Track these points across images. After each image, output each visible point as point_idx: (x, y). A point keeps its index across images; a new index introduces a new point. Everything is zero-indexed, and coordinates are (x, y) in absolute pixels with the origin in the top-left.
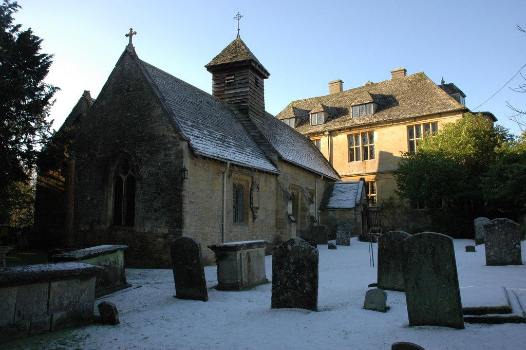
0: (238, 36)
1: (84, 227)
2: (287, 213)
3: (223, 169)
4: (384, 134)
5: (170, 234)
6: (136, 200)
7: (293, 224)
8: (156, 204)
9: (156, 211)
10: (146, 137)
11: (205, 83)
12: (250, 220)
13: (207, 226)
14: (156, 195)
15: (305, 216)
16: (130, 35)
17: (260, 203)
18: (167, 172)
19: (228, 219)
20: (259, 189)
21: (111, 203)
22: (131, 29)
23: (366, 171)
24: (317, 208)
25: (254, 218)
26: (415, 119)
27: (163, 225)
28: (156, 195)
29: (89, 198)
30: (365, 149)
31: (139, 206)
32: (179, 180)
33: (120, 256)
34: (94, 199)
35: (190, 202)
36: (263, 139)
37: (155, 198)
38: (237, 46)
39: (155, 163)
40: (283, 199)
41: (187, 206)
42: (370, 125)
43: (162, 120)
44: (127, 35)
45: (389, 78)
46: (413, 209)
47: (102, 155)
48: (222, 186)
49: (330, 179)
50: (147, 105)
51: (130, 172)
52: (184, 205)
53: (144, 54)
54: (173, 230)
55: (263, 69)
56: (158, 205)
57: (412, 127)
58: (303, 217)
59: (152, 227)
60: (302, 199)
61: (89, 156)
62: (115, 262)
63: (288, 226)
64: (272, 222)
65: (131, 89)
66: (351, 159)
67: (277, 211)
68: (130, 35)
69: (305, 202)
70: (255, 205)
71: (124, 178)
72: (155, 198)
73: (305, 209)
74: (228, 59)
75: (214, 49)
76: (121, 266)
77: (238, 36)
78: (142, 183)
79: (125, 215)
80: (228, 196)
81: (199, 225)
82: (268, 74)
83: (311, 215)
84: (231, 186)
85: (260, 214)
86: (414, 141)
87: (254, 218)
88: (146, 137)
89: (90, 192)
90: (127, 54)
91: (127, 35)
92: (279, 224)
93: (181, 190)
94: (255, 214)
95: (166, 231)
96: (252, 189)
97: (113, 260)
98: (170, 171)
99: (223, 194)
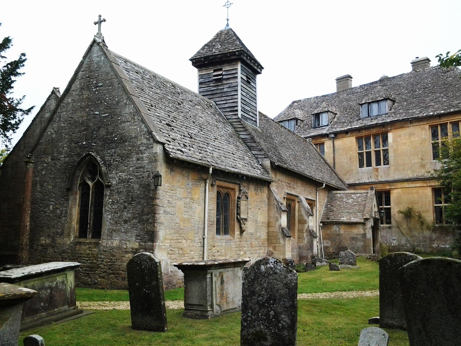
0: (228, 25)
1: (44, 241)
2: (281, 225)
3: (205, 176)
4: (400, 136)
5: (141, 249)
6: (104, 210)
7: (287, 239)
8: (126, 215)
9: (126, 222)
10: (116, 139)
11: (189, 79)
12: (237, 232)
13: (185, 239)
14: (126, 205)
15: (303, 230)
16: (99, 22)
17: (249, 214)
18: (140, 178)
19: (210, 231)
20: (248, 198)
21: (75, 212)
22: (100, 16)
23: (378, 179)
24: (319, 220)
25: (242, 231)
26: (440, 116)
27: (134, 238)
28: (126, 205)
29: (51, 207)
30: (377, 153)
31: (107, 217)
32: (153, 187)
33: (71, 277)
34: (57, 208)
35: (164, 211)
36: (255, 142)
37: (125, 207)
38: (227, 36)
39: (126, 168)
40: (275, 209)
41: (161, 216)
42: (383, 125)
43: (134, 119)
44: (96, 23)
45: (409, 69)
46: (437, 223)
47: (67, 159)
48: (204, 194)
49: (334, 188)
50: (118, 103)
51: (98, 177)
52: (157, 215)
53: (113, 47)
54: (143, 244)
55: (256, 61)
56: (129, 215)
57: (436, 126)
58: (301, 231)
59: (119, 241)
60: (299, 210)
61: (52, 159)
62: (63, 282)
63: (282, 241)
64: (263, 235)
65: (100, 85)
66: (361, 166)
67: (269, 223)
68: (99, 22)
69: (303, 213)
70: (243, 216)
71: (90, 183)
72: (125, 207)
73: (302, 222)
74: (217, 50)
75: (199, 38)
76: (71, 288)
77: (228, 25)
78: (111, 191)
79: (91, 225)
80: (211, 206)
81: (175, 238)
82: (262, 68)
83: (310, 229)
84: (214, 195)
85: (249, 227)
86: (380, 151)
87: (242, 231)
88: (116, 139)
89: (53, 200)
90: (95, 45)
91: (96, 23)
92: (271, 239)
93: (154, 198)
94: (243, 226)
95: (136, 245)
96: (239, 198)
97: (61, 281)
98: (143, 177)
99: (205, 202)
